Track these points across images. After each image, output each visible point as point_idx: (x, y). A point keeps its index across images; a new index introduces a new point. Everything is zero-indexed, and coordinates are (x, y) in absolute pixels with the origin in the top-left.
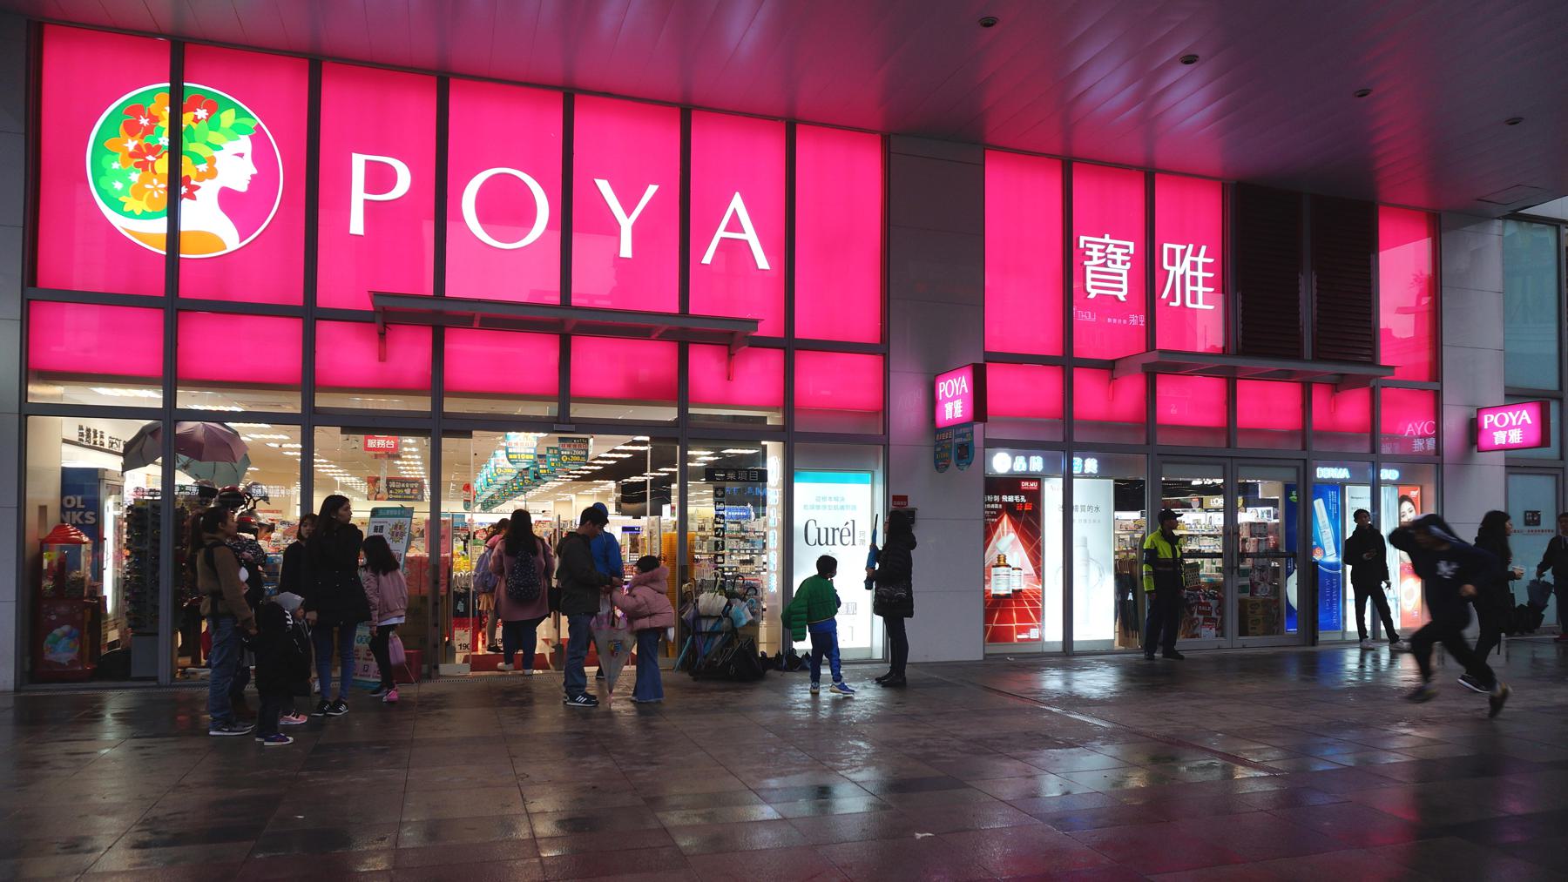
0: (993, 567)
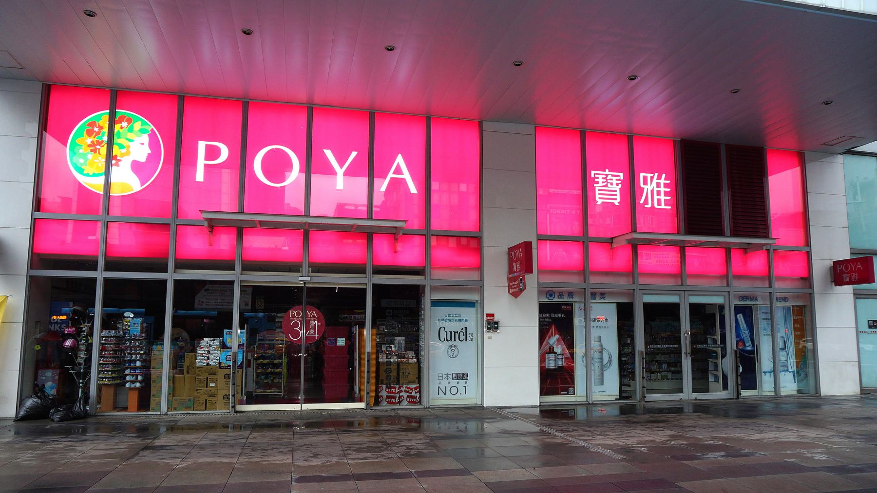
0: (547, 353)
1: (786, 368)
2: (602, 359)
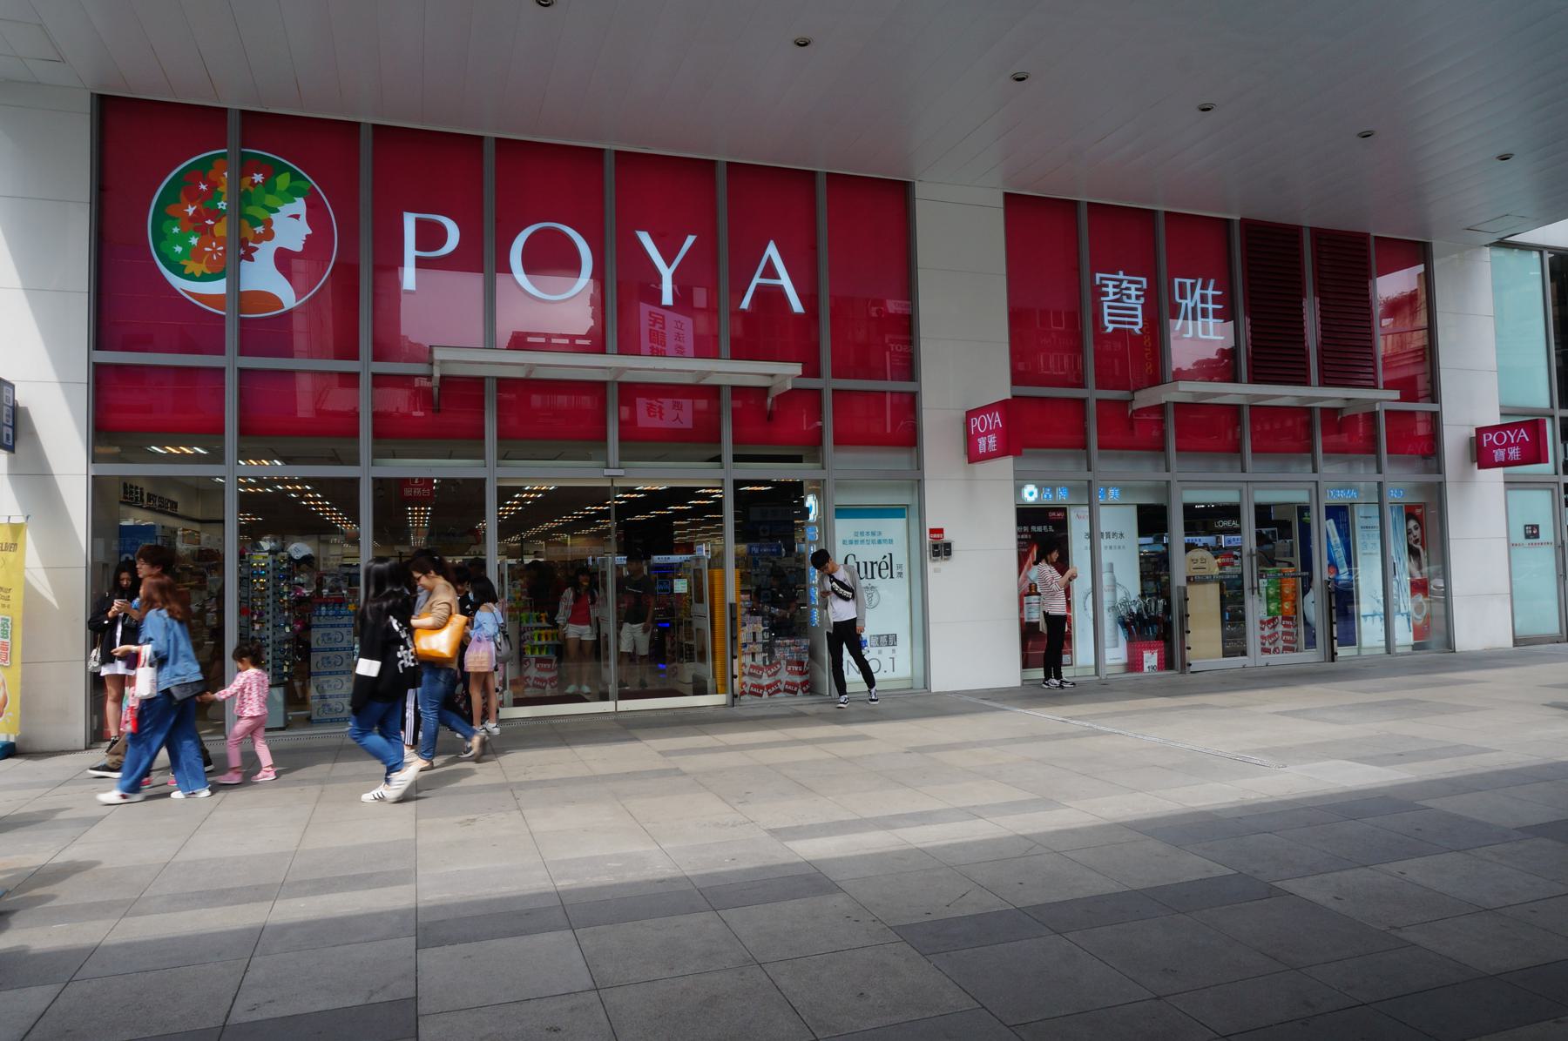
0: (1025, 595)
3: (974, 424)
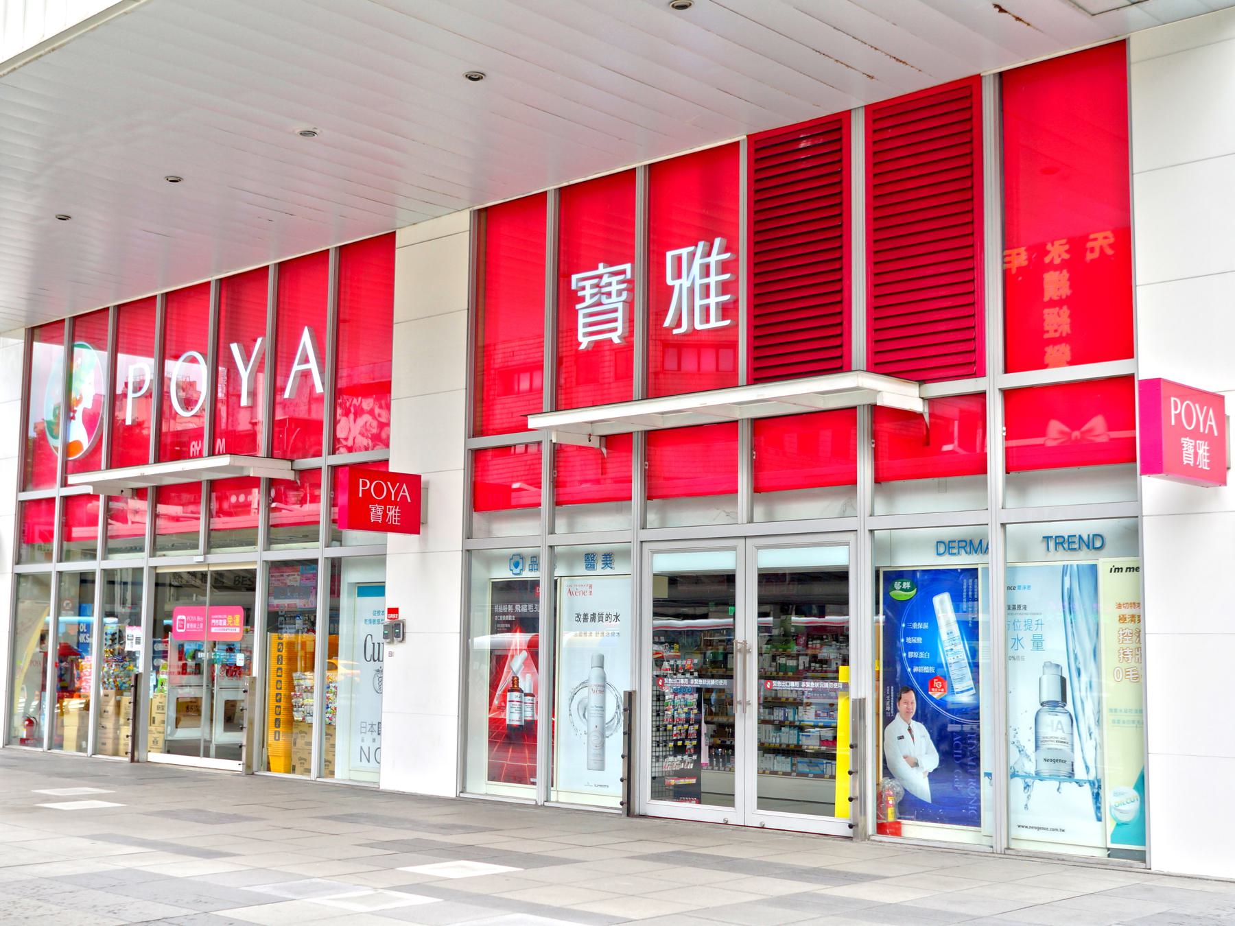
0: (509, 691)
1: (1065, 769)
2: (602, 708)
3: (1176, 409)
